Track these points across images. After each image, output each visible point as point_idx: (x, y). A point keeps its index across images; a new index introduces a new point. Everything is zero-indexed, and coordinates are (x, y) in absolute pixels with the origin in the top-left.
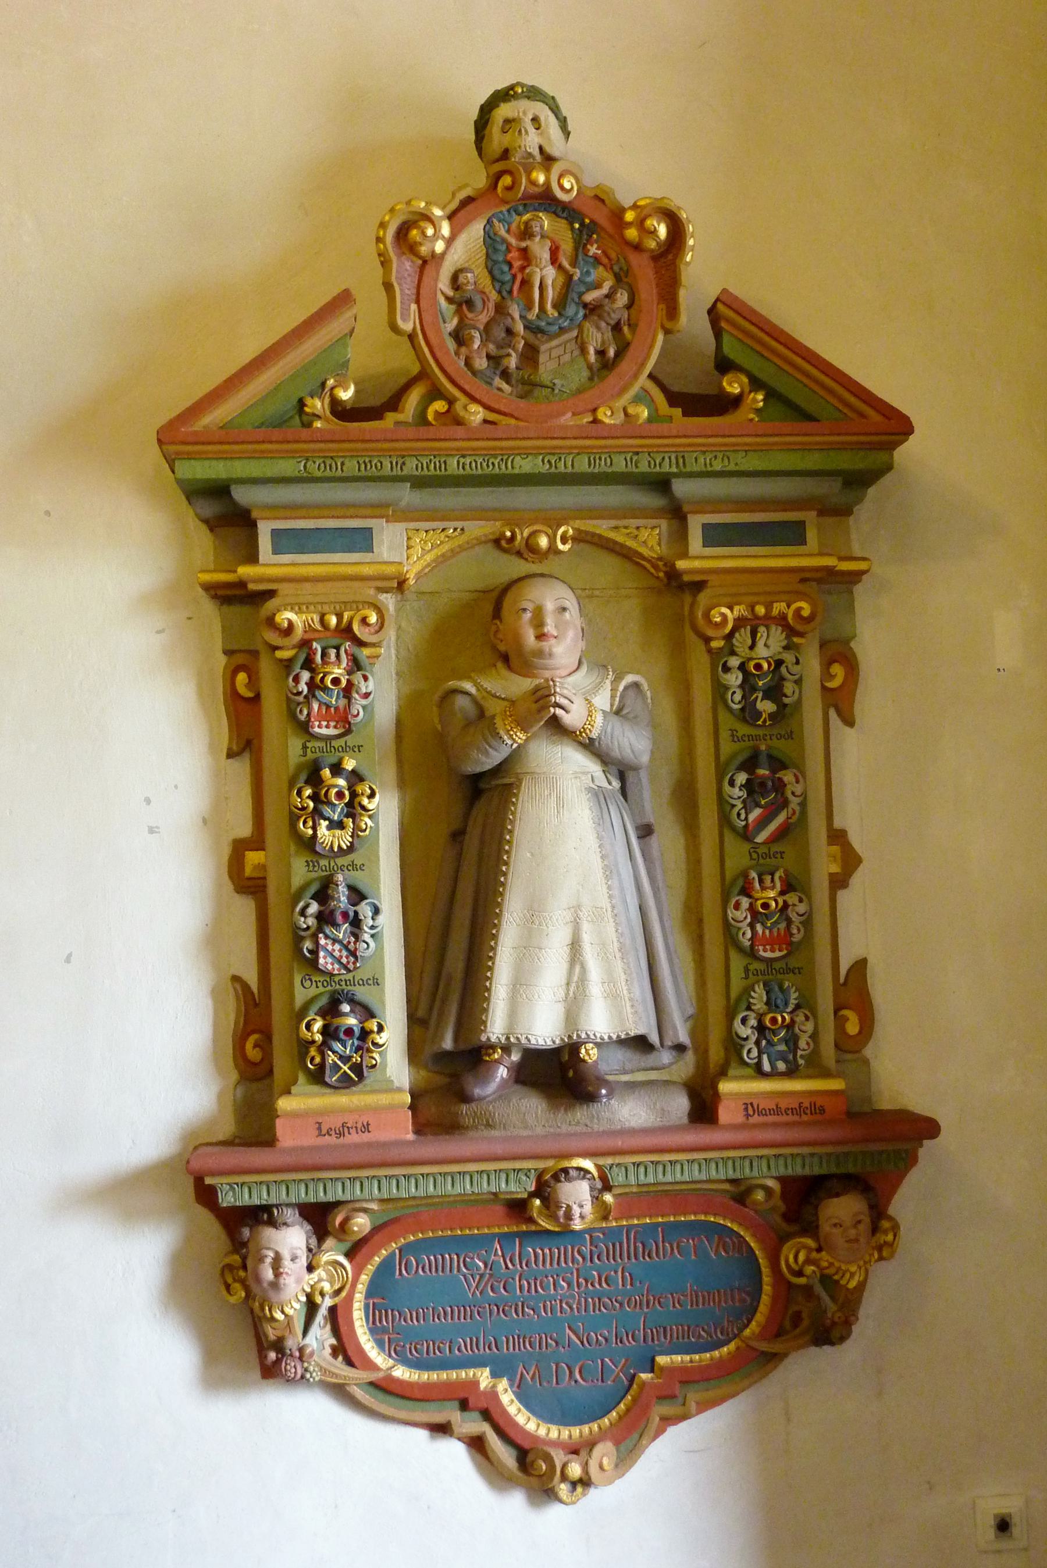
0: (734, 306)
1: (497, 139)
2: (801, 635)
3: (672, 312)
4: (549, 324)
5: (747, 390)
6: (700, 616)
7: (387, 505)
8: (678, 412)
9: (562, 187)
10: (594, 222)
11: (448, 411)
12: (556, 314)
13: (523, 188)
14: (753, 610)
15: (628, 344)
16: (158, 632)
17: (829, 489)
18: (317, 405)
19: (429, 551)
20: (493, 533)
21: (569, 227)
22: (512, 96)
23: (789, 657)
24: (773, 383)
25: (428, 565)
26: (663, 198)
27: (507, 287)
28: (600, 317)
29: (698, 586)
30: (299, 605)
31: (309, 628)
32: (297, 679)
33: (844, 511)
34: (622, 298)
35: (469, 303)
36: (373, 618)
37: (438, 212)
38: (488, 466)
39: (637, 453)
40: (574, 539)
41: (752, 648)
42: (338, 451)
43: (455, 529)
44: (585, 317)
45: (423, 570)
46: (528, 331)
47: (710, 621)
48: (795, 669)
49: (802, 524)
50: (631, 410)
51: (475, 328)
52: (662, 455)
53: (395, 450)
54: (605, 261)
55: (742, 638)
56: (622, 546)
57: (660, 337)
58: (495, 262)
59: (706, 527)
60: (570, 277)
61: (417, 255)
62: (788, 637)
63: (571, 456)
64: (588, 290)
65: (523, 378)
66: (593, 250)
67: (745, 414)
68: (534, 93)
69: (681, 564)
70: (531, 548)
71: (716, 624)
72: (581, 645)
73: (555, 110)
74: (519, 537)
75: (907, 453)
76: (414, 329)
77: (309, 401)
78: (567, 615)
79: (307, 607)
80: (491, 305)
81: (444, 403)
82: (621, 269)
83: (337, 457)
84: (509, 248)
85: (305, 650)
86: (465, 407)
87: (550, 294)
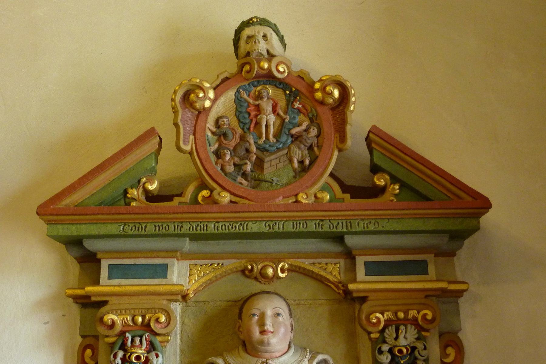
0: (380, 135)
1: (243, 47)
2: (427, 331)
3: (343, 138)
4: (270, 146)
5: (388, 184)
6: (364, 318)
7: (176, 251)
8: (348, 196)
9: (278, 71)
10: (297, 90)
11: (210, 196)
12: (275, 141)
13: (255, 71)
14: (396, 313)
15: (317, 157)
16: (45, 323)
17: (442, 241)
18: (134, 193)
19: (202, 277)
20: (241, 266)
21: (283, 93)
22: (251, 24)
23: (420, 345)
24: (405, 179)
25: (201, 286)
26: (336, 75)
27: (247, 126)
28: (301, 142)
29: (363, 300)
30: (121, 310)
31: (125, 324)
32: (115, 356)
33: (452, 254)
34: (314, 132)
35: (225, 135)
36: (163, 319)
37: (207, 85)
38: (232, 228)
39: (322, 220)
40: (289, 270)
41: (396, 338)
42: (143, 219)
43: (218, 264)
44: (292, 142)
45: (198, 288)
46: (258, 151)
47: (370, 322)
48: (424, 353)
49: (425, 262)
50: (319, 195)
51: (228, 149)
52: (337, 222)
53: (176, 218)
54: (304, 111)
55: (390, 332)
56: (317, 274)
57: (336, 153)
58: (241, 112)
59: (366, 263)
60: (283, 120)
61: (194, 108)
62: (419, 332)
63: (282, 222)
64: (294, 127)
65: (255, 176)
66: (297, 105)
67: (388, 197)
68: (264, 22)
69: (351, 287)
70: (263, 275)
71: (374, 324)
72: (290, 336)
73: (277, 31)
74: (255, 269)
75: (488, 219)
76: (192, 149)
77: (130, 191)
78: (280, 318)
79: (125, 312)
80: (238, 136)
81: (208, 191)
82: (313, 115)
83: (143, 223)
84: (249, 105)
85: (122, 338)
86: (219, 194)
87: (272, 130)
